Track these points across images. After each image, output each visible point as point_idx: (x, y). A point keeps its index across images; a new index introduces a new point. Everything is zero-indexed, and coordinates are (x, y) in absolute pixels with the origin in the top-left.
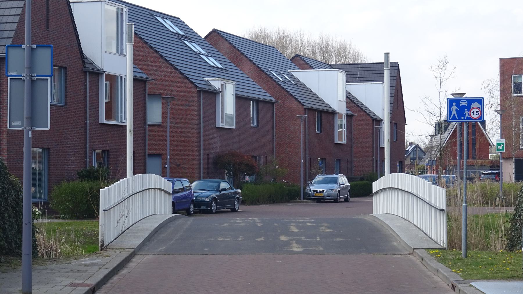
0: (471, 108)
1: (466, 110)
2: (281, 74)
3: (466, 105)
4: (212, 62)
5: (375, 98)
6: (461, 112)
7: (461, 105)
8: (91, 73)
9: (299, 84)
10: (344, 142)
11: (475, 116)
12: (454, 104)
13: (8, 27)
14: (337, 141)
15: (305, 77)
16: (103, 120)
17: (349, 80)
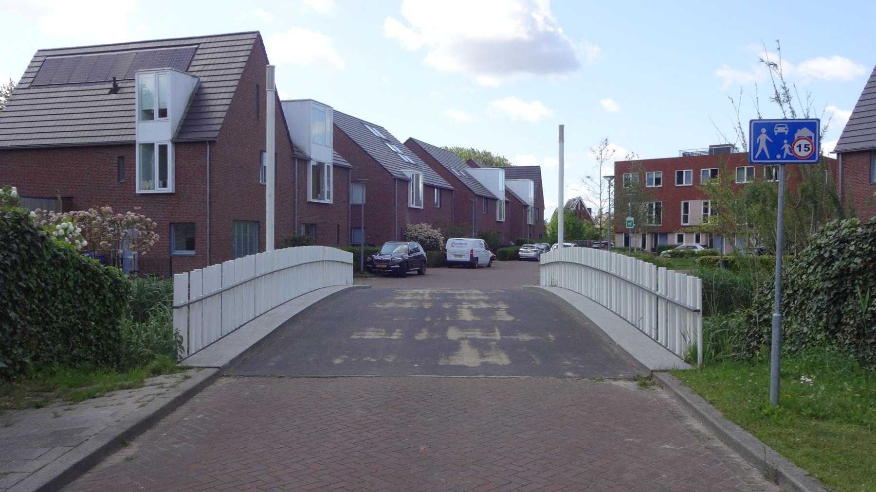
0: (796, 138)
1: (785, 141)
2: (459, 171)
3: (786, 132)
4: (407, 159)
5: (525, 190)
6: (775, 144)
7: (776, 132)
8: (299, 159)
9: (471, 178)
10: (503, 220)
11: (803, 154)
12: (764, 130)
13: (219, 115)
14: (498, 219)
15: (475, 173)
16: (310, 198)
17: (508, 177)
